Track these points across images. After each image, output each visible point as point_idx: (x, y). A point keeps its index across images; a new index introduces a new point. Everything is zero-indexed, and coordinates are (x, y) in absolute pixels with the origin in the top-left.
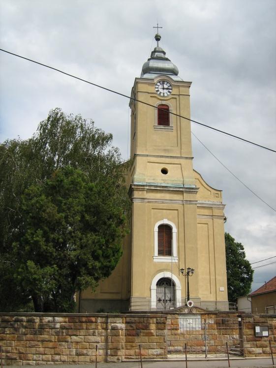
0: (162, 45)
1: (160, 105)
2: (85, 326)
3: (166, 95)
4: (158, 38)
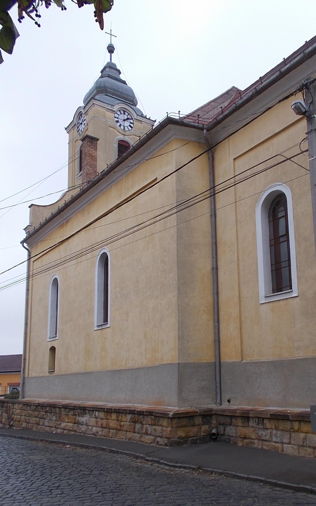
0: (116, 59)
1: (119, 141)
3: (126, 129)
4: (111, 49)
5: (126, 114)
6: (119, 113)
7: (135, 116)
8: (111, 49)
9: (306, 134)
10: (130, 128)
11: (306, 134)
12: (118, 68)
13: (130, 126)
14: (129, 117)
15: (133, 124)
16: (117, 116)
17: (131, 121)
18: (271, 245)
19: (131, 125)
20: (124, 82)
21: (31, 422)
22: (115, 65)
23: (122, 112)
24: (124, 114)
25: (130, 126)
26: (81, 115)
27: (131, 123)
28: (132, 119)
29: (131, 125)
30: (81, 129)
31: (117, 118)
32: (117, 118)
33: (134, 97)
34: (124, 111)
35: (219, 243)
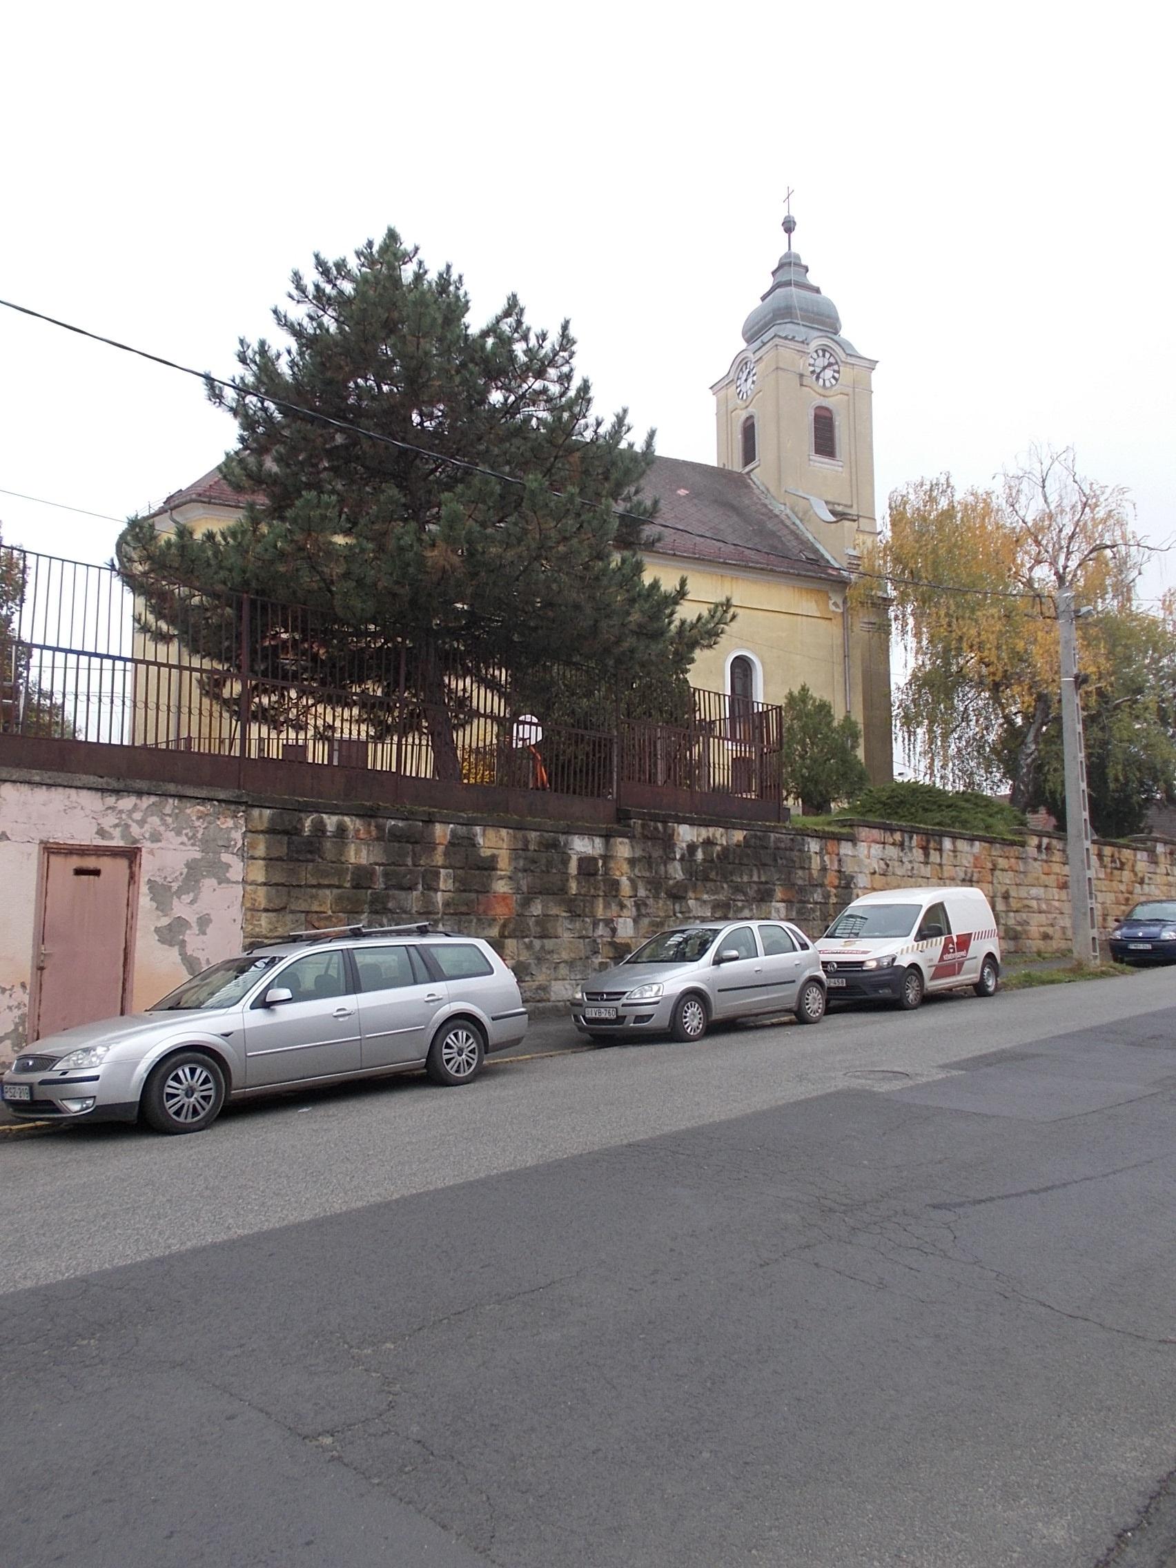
0: (802, 245)
2: (267, 699)
3: (828, 384)
4: (789, 226)
5: (827, 355)
6: (815, 355)
7: (843, 356)
8: (789, 226)
9: (262, 344)
10: (833, 382)
11: (262, 344)
12: (804, 262)
13: (834, 377)
14: (832, 360)
15: (838, 372)
16: (812, 361)
17: (836, 367)
18: (422, 972)
19: (836, 375)
20: (817, 291)
21: (261, 836)
22: (798, 257)
23: (820, 353)
24: (824, 356)
25: (834, 377)
26: (746, 363)
27: (835, 371)
28: (837, 363)
29: (836, 375)
30: (744, 390)
31: (813, 365)
32: (813, 365)
33: (837, 319)
34: (824, 351)
35: (73, 837)
